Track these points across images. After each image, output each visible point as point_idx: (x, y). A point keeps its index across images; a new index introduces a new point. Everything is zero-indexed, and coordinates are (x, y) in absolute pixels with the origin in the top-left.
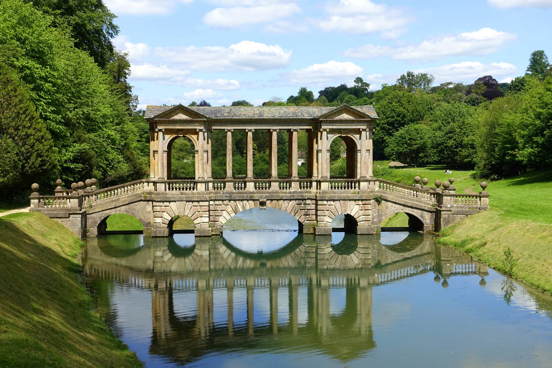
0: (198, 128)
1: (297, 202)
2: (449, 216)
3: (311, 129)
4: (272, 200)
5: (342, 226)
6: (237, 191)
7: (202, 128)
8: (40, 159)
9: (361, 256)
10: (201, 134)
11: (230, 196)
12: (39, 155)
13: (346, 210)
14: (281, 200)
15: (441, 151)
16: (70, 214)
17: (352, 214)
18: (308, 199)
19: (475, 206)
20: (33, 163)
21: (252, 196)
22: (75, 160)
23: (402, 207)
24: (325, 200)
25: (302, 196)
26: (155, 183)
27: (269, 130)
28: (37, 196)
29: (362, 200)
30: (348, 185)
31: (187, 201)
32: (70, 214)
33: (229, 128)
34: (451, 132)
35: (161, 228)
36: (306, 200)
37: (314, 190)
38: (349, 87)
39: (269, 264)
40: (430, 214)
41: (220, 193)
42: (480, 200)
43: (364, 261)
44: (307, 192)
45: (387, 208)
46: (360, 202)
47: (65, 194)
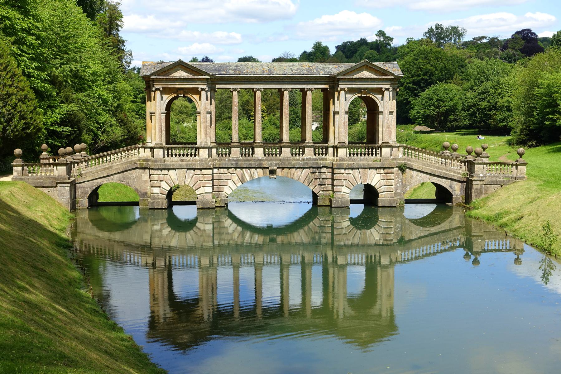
1: (311, 170)
2: (481, 187)
4: (283, 168)
7: (205, 86)
11: (236, 164)
12: (22, 118)
13: (366, 180)
14: (293, 168)
15: (473, 114)
16: (57, 183)
17: (373, 184)
18: (323, 167)
19: (511, 176)
20: (15, 127)
21: (261, 164)
22: (63, 122)
23: (429, 176)
24: (342, 168)
25: (317, 163)
26: (152, 149)
27: (280, 89)
28: (21, 163)
29: (384, 168)
30: (368, 151)
31: (188, 169)
32: (57, 183)
34: (484, 93)
35: (158, 198)
36: (321, 168)
37: (330, 156)
38: (369, 41)
39: (279, 239)
40: (460, 184)
41: (225, 160)
42: (517, 169)
44: (322, 159)
45: (412, 177)
46: (382, 171)
47: (51, 161)
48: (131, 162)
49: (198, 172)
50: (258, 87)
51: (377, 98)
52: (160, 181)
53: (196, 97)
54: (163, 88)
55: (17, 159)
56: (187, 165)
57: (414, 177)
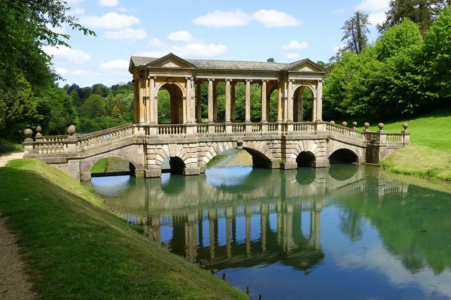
0: (187, 76)
1: (267, 142)
2: (385, 150)
3: (277, 80)
4: (247, 141)
5: (169, 167)
6: (218, 134)
7: (190, 76)
8: (23, 106)
9: (317, 185)
10: (189, 81)
11: (213, 138)
14: (254, 140)
16: (68, 159)
18: (276, 139)
19: (400, 142)
20: (17, 110)
21: (232, 138)
23: (343, 144)
24: (291, 140)
25: (271, 137)
26: (147, 128)
29: (319, 139)
30: (172, 130)
31: (178, 144)
32: (68, 159)
33: (211, 77)
35: (154, 169)
36: (273, 140)
37: (280, 132)
39: (245, 196)
40: (362, 149)
41: (203, 136)
42: (404, 137)
43: (320, 189)
44: (274, 134)
45: (333, 145)
46: (318, 141)
47: (45, 140)
48: (127, 139)
49: (186, 146)
50: (228, 78)
51: (181, 85)
52: (156, 154)
53: (183, 85)
54: (157, 77)
55: (27, 139)
56: (177, 140)
57: (334, 145)
